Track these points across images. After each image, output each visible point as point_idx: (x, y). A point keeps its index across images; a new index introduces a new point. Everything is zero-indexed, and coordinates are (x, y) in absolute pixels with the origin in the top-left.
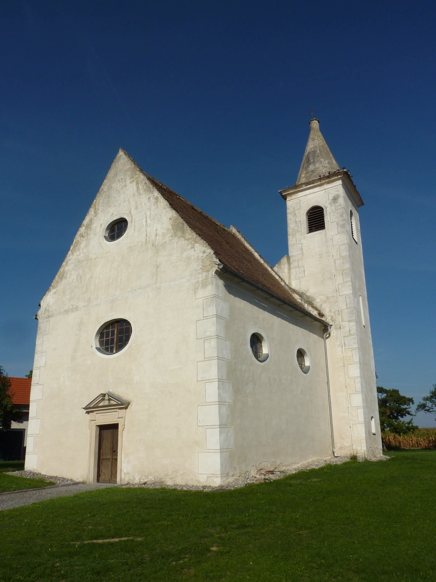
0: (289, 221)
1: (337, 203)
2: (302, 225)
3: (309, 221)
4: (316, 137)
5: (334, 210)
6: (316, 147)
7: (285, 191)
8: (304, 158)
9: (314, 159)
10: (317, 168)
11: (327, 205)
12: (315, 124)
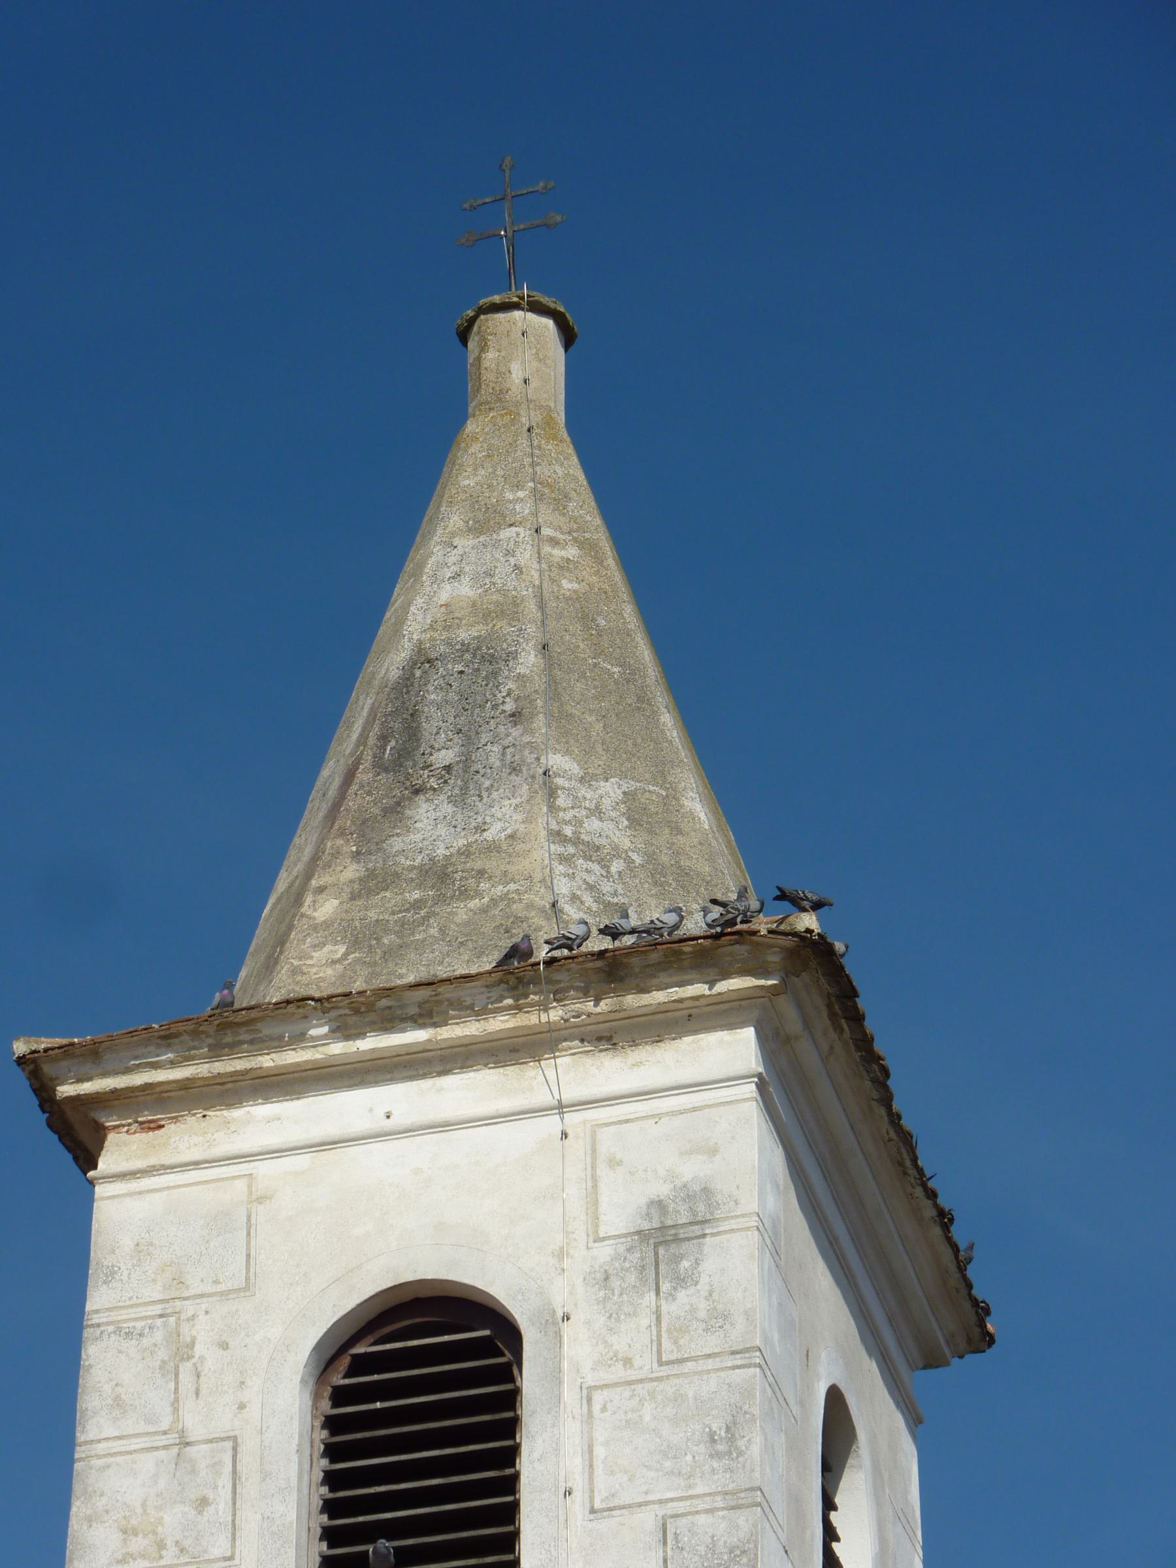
0: (100, 1427)
1: (681, 1281)
2: (250, 1488)
3: (332, 1452)
4: (520, 501)
5: (645, 1363)
6: (509, 609)
7: (93, 1056)
8: (362, 707)
9: (468, 736)
10: (492, 848)
11: (568, 1290)
12: (524, 355)
